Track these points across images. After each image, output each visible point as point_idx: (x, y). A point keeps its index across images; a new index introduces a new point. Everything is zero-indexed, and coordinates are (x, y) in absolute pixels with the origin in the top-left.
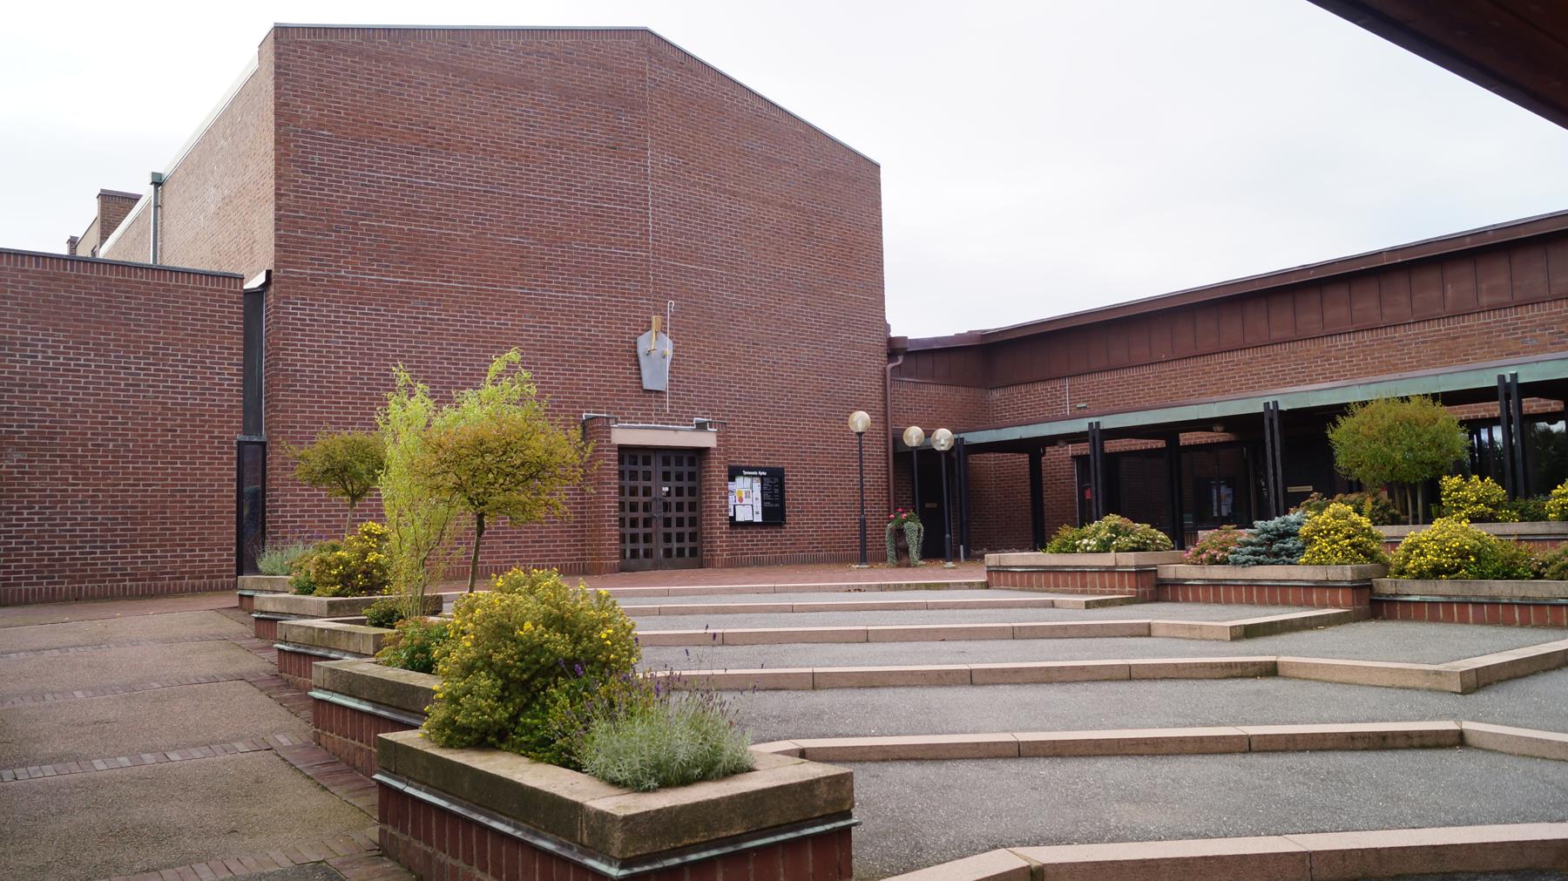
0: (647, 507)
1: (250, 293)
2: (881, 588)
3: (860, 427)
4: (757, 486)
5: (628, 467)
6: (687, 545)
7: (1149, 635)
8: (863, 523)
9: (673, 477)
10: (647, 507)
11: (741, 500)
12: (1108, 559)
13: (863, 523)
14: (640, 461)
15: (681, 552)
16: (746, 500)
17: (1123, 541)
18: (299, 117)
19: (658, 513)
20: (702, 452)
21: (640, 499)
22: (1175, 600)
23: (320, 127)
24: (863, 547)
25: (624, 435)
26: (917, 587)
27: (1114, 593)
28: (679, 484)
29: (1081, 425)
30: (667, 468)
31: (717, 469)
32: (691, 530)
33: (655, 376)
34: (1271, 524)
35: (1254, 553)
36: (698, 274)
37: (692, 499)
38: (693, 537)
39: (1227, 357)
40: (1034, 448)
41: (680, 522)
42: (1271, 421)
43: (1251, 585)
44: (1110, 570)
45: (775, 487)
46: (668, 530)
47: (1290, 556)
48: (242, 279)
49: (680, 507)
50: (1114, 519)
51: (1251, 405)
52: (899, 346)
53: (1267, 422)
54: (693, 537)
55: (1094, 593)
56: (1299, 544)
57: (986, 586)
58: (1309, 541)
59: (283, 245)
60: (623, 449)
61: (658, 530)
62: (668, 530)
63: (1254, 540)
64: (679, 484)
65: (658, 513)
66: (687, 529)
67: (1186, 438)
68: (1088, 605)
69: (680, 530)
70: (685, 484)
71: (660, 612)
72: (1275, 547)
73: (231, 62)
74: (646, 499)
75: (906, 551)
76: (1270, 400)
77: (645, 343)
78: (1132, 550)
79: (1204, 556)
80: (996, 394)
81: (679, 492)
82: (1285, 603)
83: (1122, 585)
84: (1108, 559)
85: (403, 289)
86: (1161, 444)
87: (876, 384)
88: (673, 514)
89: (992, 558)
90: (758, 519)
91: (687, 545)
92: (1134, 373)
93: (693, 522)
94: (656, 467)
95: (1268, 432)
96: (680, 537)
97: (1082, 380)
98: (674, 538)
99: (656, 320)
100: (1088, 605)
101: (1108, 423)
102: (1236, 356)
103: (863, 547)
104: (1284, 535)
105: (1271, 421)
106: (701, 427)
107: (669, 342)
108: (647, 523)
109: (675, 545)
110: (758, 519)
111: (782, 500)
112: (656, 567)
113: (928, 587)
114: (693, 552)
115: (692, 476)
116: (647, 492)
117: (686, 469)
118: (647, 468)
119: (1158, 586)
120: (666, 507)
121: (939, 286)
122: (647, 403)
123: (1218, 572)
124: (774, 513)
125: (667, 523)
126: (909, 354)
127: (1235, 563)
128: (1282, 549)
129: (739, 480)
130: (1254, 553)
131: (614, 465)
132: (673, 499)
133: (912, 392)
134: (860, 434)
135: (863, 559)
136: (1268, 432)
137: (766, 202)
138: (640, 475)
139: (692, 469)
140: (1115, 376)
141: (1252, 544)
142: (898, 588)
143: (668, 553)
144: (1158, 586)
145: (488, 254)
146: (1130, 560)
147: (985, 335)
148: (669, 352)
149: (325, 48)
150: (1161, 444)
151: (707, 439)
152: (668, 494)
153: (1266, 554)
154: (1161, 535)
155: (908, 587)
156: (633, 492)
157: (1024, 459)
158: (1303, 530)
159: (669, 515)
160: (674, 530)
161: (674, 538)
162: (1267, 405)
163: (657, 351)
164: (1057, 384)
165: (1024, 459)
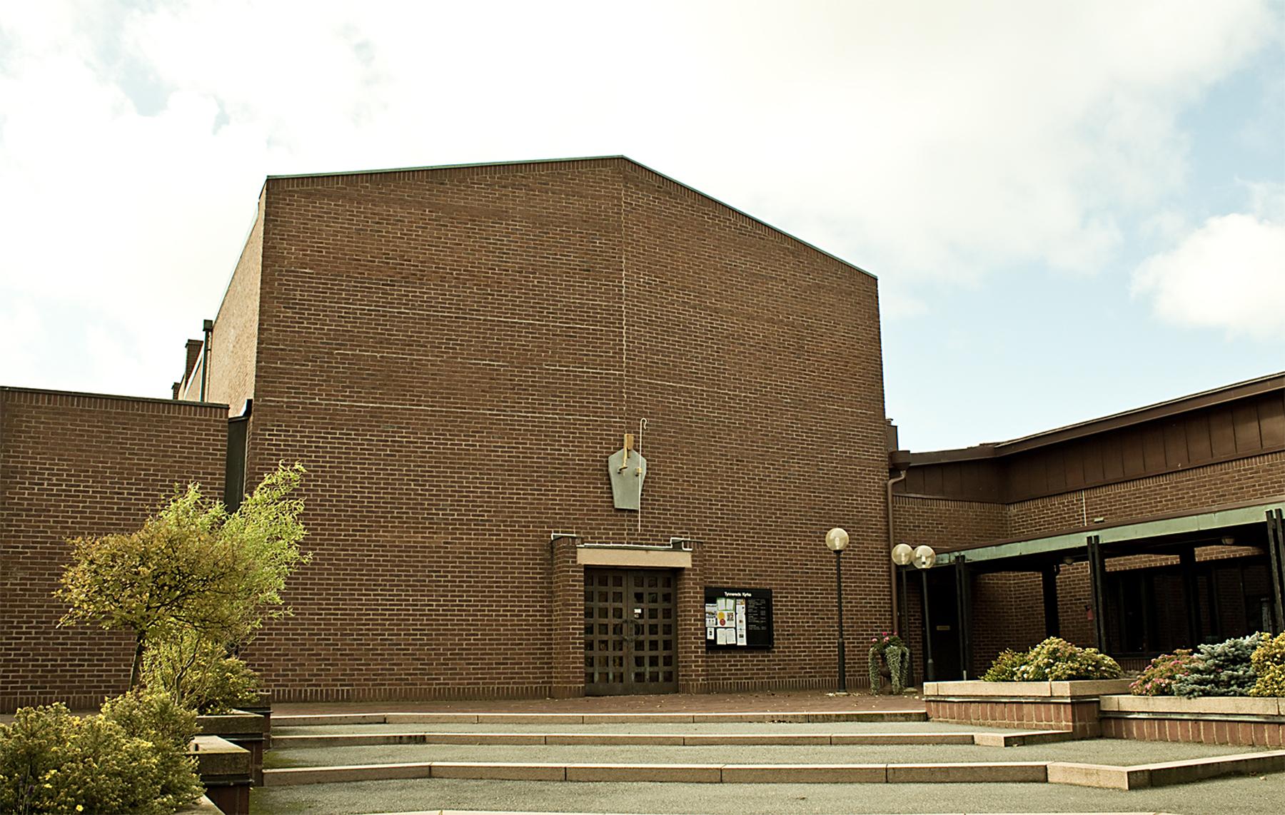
0: (618, 629)
1: (233, 421)
2: (809, 719)
3: (838, 545)
4: (741, 609)
5: (596, 588)
6: (661, 669)
7: (1046, 781)
8: (842, 646)
9: (646, 597)
10: (618, 629)
11: (723, 622)
12: (1042, 689)
13: (842, 646)
14: (610, 581)
15: (654, 678)
16: (728, 622)
17: (1060, 667)
18: (284, 258)
19: (629, 634)
20: (674, 574)
21: (611, 621)
22: (1119, 737)
23: (304, 265)
24: (842, 675)
25: (587, 556)
26: (848, 718)
27: (1051, 727)
28: (653, 606)
29: (1080, 540)
30: (640, 590)
31: (691, 591)
32: (666, 653)
33: (627, 495)
34: (1219, 648)
35: (1200, 683)
36: (676, 391)
37: (667, 621)
38: (668, 661)
39: (1245, 464)
40: (1047, 563)
41: (654, 645)
42: (1275, 531)
43: (1198, 719)
44: (1045, 701)
45: (761, 608)
46: (640, 653)
47: (1241, 685)
48: (227, 408)
49: (653, 629)
50: (1053, 642)
51: (1256, 515)
52: (900, 460)
53: (1270, 533)
54: (668, 661)
55: (1029, 728)
56: (1251, 672)
57: (925, 718)
58: (1262, 667)
59: (263, 376)
60: (589, 569)
61: (630, 652)
62: (640, 653)
63: (1201, 666)
64: (653, 606)
65: (629, 634)
66: (661, 653)
67: (1203, 554)
68: (1008, 742)
69: (654, 653)
70: (660, 606)
71: (546, 741)
72: (1224, 675)
73: (246, 212)
74: (617, 621)
75: (888, 676)
76: (1273, 508)
77: (615, 462)
78: (1070, 678)
79: (1148, 686)
80: (1013, 510)
81: (653, 614)
82: (1236, 743)
83: (1058, 719)
84: (1042, 689)
85: (374, 413)
86: (1174, 560)
87: (878, 501)
88: (646, 637)
89: (930, 687)
90: (743, 642)
91: (661, 669)
92: (1150, 483)
93: (667, 645)
94: (629, 589)
95: (1272, 543)
96: (654, 662)
97: (1098, 492)
98: (647, 661)
99: (628, 439)
100: (1008, 742)
101: (1107, 537)
102: (1256, 463)
103: (842, 675)
104: (1240, 659)
105: (1275, 531)
106: (677, 547)
107: (642, 460)
108: (619, 645)
109: (647, 669)
110: (743, 642)
111: (769, 623)
112: (626, 692)
113: (860, 718)
114: (669, 677)
115: (667, 598)
116: (618, 613)
117: (660, 590)
118: (619, 589)
119: (1101, 720)
120: (639, 629)
121: (942, 401)
122: (620, 525)
123: (1163, 704)
124: (760, 637)
125: (639, 645)
126: (910, 469)
127: (1180, 693)
128: (1231, 677)
129: (721, 602)
130: (1200, 683)
131: (580, 586)
132: (647, 621)
133: (916, 506)
134: (838, 552)
135: (842, 686)
136: (1272, 543)
137: (750, 318)
138: (610, 596)
139: (667, 590)
140: (1131, 487)
141: (1198, 671)
142: (827, 719)
143: (640, 677)
144: (1101, 720)
145: (458, 377)
146: (1063, 689)
147: (996, 448)
148: (643, 471)
149: (311, 194)
150: (1174, 560)
151: (682, 560)
152: (641, 616)
153: (1217, 683)
154: (1109, 660)
155: (838, 718)
156: (604, 613)
157: (1038, 577)
158: (1254, 656)
159: (641, 638)
160: (647, 653)
161: (647, 661)
162: (1269, 513)
163: (629, 469)
164: (1074, 497)
165: (1038, 577)
